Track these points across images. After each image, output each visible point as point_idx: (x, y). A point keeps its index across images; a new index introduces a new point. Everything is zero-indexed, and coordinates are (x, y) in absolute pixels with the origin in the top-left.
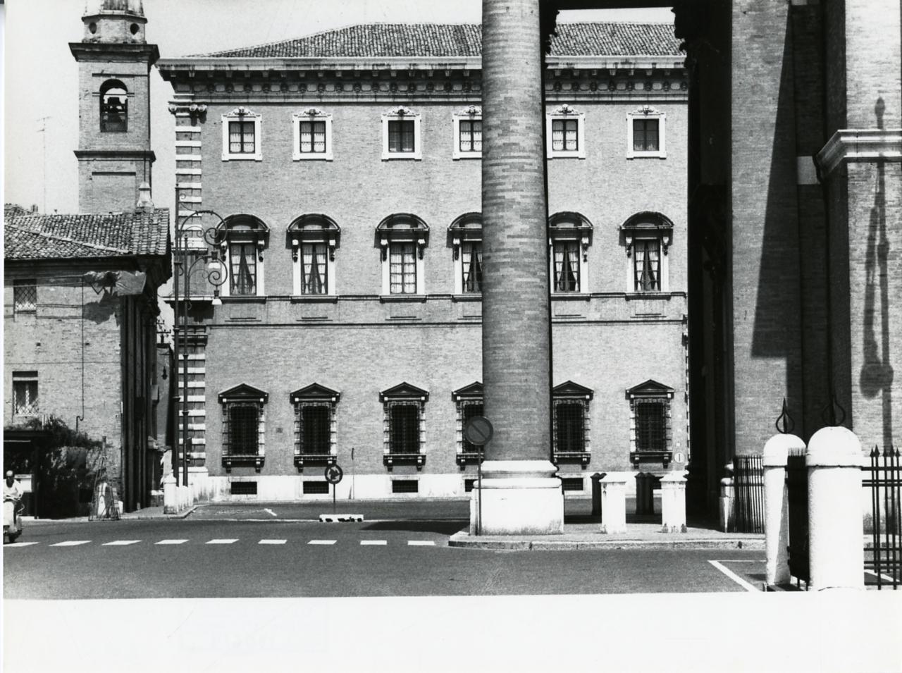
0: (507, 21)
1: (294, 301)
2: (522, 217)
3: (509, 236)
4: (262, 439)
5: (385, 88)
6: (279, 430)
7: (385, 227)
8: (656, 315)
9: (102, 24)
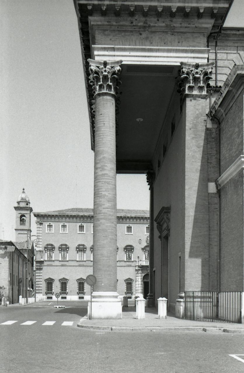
0: (104, 128)
1: (60, 261)
2: (108, 201)
3: (104, 208)
4: (53, 288)
5: (78, 219)
6: (56, 287)
7: (78, 247)
8: (130, 265)
9: (21, 203)
